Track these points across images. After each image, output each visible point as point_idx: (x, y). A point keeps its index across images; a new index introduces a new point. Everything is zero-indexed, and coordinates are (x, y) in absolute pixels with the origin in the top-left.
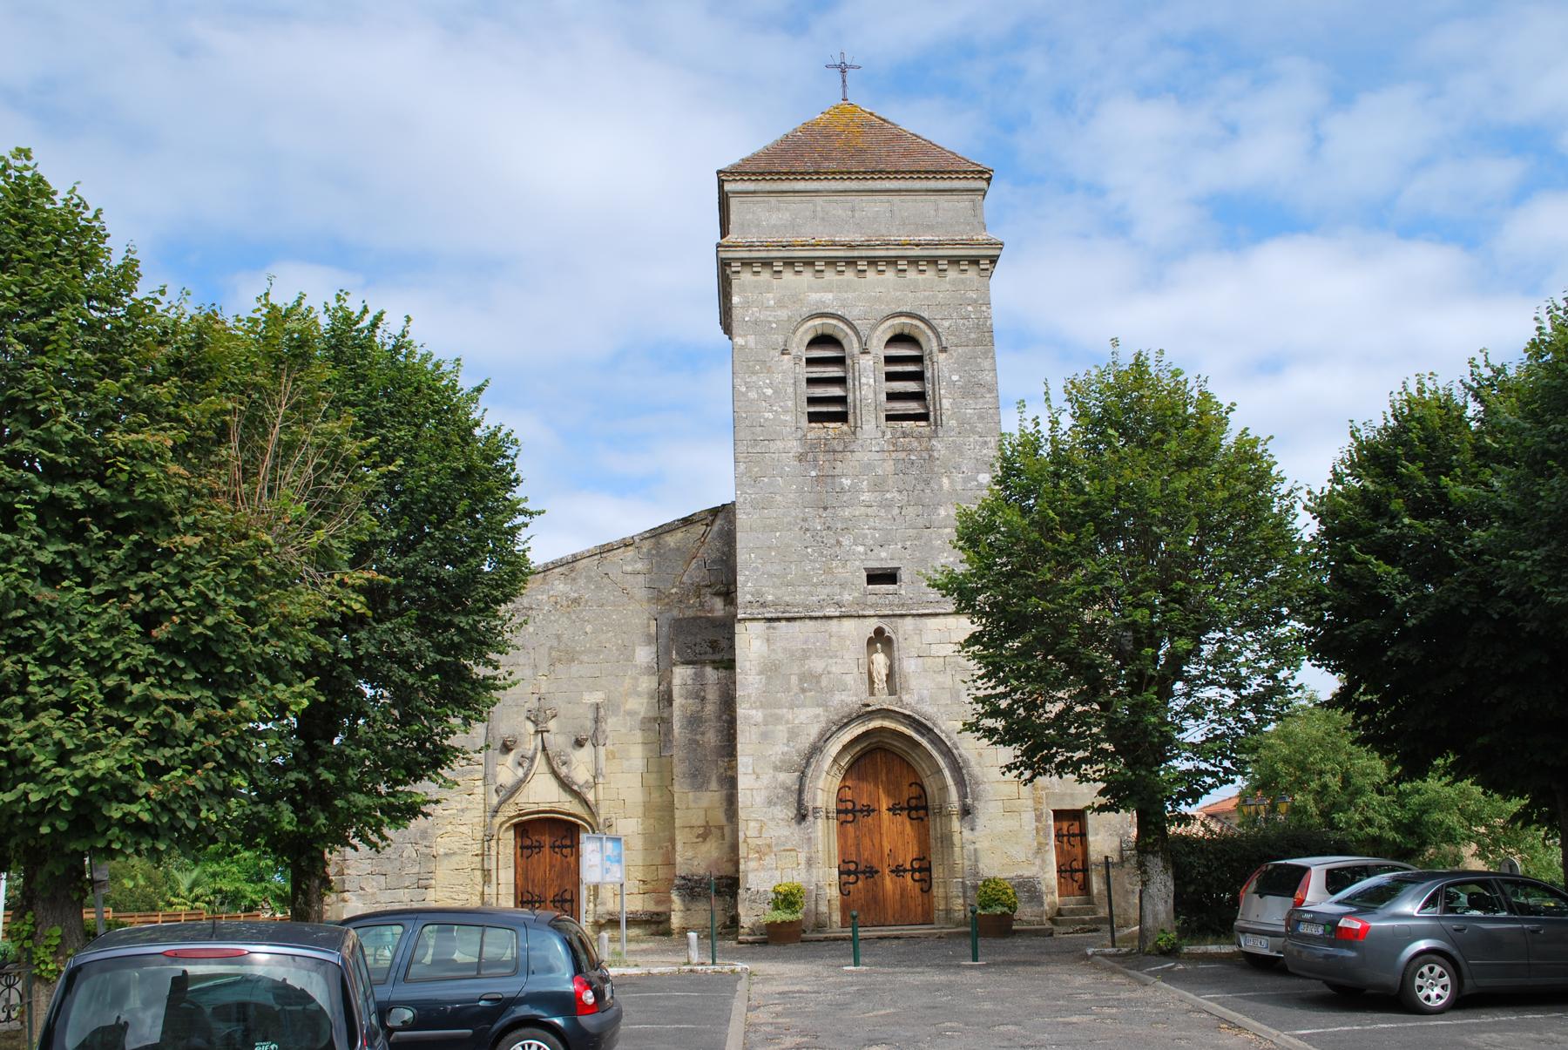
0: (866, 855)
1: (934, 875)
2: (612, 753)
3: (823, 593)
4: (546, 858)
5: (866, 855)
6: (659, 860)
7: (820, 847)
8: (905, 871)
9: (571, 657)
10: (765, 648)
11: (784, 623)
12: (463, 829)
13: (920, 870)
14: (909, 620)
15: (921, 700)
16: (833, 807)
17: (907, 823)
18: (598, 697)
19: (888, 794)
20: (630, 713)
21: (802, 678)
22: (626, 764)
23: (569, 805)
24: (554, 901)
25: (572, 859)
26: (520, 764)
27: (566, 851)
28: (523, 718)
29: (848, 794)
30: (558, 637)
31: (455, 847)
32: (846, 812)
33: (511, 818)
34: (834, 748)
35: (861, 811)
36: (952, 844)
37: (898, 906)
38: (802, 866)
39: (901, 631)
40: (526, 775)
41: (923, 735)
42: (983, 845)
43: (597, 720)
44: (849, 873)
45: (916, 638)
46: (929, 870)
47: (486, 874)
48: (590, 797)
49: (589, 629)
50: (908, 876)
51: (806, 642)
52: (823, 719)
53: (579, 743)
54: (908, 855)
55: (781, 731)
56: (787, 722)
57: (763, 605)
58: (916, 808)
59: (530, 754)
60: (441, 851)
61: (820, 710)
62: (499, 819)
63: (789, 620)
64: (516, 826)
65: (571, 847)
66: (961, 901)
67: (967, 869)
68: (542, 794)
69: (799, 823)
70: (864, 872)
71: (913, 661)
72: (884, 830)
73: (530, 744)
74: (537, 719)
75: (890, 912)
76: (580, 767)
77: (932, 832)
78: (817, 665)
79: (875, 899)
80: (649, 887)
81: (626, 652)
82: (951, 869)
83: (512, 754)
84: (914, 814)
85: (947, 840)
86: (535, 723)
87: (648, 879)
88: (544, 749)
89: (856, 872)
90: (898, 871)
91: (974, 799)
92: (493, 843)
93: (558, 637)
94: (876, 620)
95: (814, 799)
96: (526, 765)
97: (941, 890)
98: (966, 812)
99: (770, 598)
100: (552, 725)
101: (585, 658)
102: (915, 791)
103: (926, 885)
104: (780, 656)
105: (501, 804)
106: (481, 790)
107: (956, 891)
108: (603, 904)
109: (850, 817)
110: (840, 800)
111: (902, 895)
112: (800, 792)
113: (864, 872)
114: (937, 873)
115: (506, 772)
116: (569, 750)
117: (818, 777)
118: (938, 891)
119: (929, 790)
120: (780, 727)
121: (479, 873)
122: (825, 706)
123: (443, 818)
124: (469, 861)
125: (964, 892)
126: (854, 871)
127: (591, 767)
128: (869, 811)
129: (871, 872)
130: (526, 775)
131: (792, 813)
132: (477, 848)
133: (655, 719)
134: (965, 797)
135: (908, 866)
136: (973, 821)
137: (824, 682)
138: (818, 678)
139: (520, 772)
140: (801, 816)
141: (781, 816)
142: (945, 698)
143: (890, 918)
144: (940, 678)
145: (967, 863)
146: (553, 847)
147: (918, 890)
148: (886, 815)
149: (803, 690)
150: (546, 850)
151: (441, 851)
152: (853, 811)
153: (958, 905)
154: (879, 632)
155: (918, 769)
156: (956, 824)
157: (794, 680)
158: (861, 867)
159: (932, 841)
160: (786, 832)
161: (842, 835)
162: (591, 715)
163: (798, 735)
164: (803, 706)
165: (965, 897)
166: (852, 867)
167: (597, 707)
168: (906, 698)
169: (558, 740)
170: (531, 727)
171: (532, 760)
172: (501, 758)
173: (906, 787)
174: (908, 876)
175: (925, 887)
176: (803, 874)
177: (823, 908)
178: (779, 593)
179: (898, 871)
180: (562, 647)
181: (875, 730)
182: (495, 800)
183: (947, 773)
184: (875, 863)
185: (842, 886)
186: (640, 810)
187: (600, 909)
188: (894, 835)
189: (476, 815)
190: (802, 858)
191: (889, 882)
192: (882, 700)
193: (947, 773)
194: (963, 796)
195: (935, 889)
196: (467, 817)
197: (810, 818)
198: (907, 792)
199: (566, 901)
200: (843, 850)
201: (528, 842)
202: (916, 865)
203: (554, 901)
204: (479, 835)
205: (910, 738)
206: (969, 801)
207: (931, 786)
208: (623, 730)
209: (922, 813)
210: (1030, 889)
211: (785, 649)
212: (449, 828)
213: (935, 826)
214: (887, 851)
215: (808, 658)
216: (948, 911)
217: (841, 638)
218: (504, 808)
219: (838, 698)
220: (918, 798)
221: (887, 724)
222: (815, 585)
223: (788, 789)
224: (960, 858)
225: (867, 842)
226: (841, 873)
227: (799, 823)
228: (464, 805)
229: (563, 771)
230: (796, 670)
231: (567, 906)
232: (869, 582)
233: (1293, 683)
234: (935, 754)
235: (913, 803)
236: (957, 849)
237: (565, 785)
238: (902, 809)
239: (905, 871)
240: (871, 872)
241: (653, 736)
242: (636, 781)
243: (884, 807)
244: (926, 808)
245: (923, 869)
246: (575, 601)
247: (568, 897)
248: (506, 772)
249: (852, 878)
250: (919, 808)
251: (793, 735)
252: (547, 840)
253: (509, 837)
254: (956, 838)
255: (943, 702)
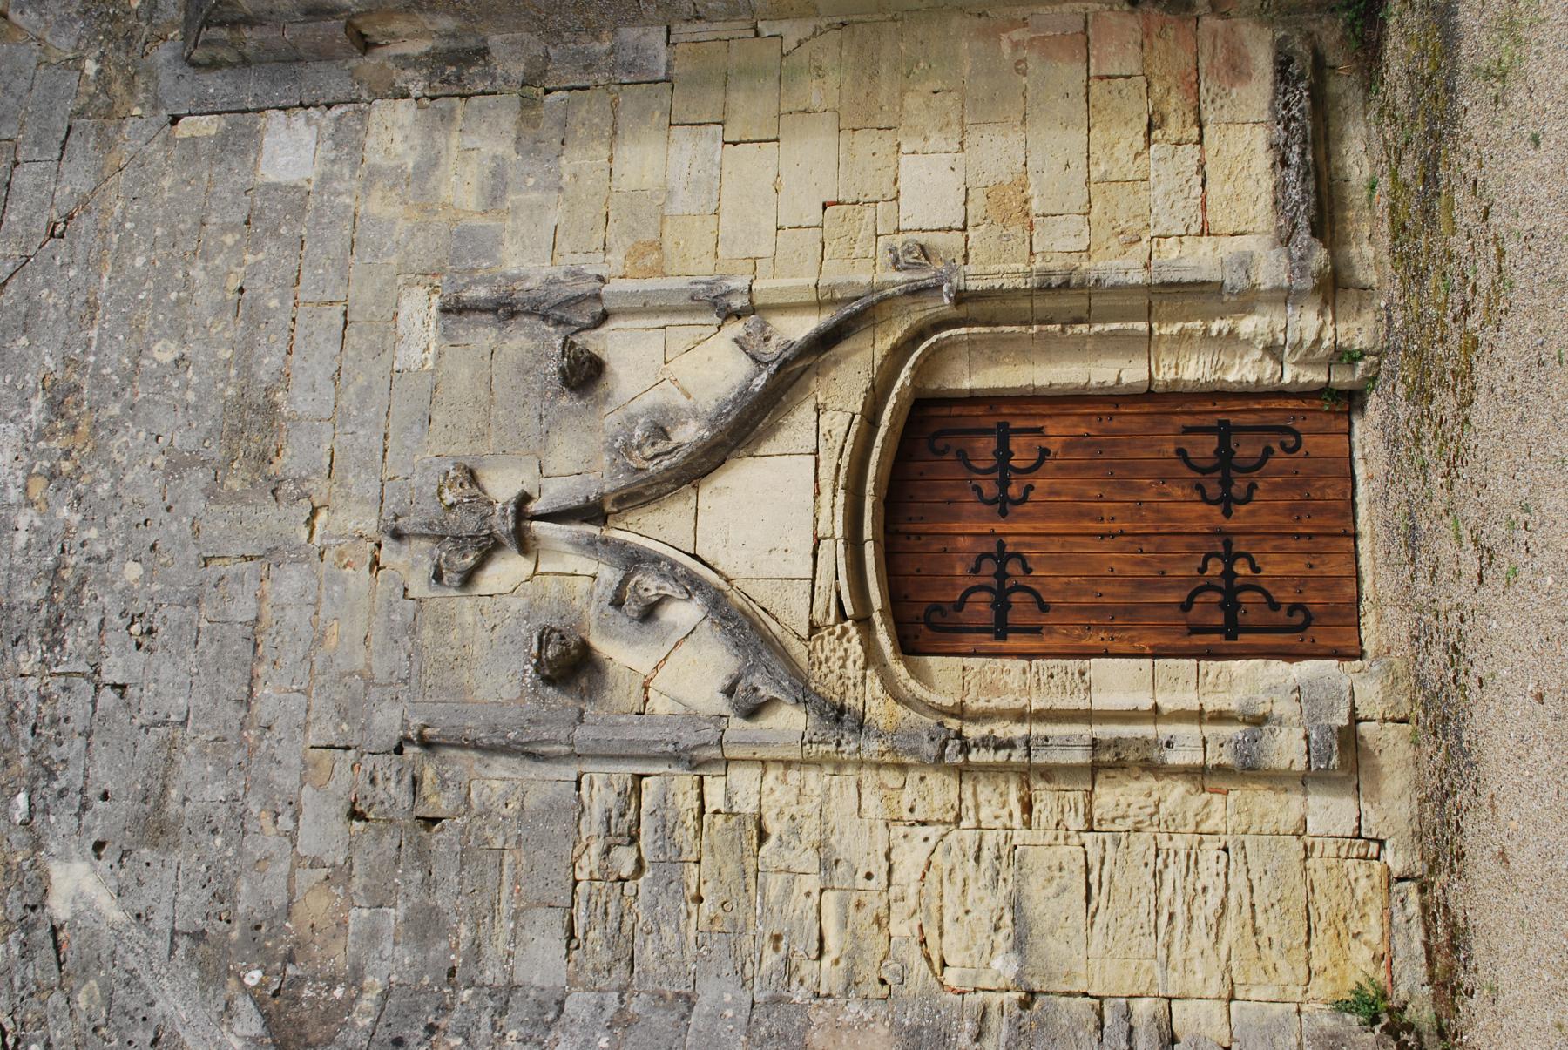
2: (638, 252)
4: (1055, 531)
6: (1069, 74)
9: (255, 418)
12: (909, 860)
18: (418, 310)
20: (496, 190)
22: (683, 202)
23: (844, 388)
24: (1227, 503)
25: (1057, 430)
26: (649, 613)
27: (1022, 451)
28: (464, 607)
30: (178, 465)
31: (987, 903)
33: (872, 656)
40: (694, 585)
43: (505, 310)
47: (1108, 762)
48: (799, 328)
49: (164, 352)
53: (584, 375)
59: (610, 575)
60: (1004, 966)
62: (879, 708)
63: (332, 747)
64: (908, 647)
65: (1004, 434)
68: (776, 522)
73: (571, 572)
74: (478, 539)
76: (680, 372)
80: (1174, 105)
81: (274, 215)
83: (604, 647)
86: (489, 549)
87: (1139, 110)
88: (591, 512)
92: (973, 731)
93: (178, 465)
96: (651, 585)
100: (502, 486)
101: (269, 362)
105: (805, 694)
106: (744, 780)
108: (1245, 263)
115: (677, 670)
116: (610, 420)
121: (1109, 797)
123: (853, 956)
124: (1051, 848)
127: (683, 331)
130: (694, 585)
132: (995, 803)
133: (528, 103)
139: (684, 613)
146: (1003, 506)
150: (1014, 528)
151: (1004, 966)
162: (484, 335)
167: (455, 309)
169: (573, 463)
170: (507, 570)
171: (634, 560)
172: (622, 693)
180: (216, 451)
182: (789, 720)
186: (866, 143)
187: (1270, 270)
189: (853, 809)
196: (858, 844)
199: (1225, 453)
201: (981, 607)
203: (1227, 503)
204: (938, 791)
208: (556, 215)
212: (901, 927)
218: (828, 684)
228: (807, 860)
229: (689, 434)
231: (1246, 449)
237: (745, 426)
241: (590, 110)
242: (753, 164)
246: (56, 407)
247: (1206, 447)
248: (677, 670)
252: (971, 528)
253: (949, 677)
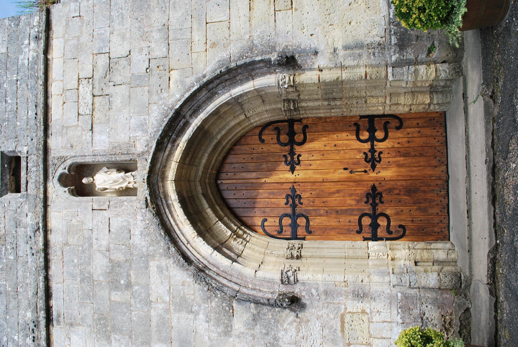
0: (351, 202)
1: (380, 110)
3: (24, 249)
5: (351, 202)
7: (339, 278)
8: (372, 150)
10: (81, 330)
11: (53, 302)
13: (372, 130)
14: (52, 142)
15: (142, 126)
16: (281, 246)
17: (308, 146)
19: (271, 170)
21: (114, 285)
29: (272, 223)
32: (294, 226)
34: (200, 249)
35: (294, 206)
36: (338, 83)
37: (422, 161)
38: (366, 306)
39: (64, 153)
41: (187, 124)
42: (339, 38)
44: (375, 226)
45: (71, 133)
46: (371, 118)
50: (379, 146)
51: (73, 277)
52: (165, 262)
54: (351, 146)
55: (180, 320)
56: (167, 311)
57: (36, 325)
58: (292, 134)
61: (153, 265)
66: (422, 69)
67: (373, 61)
69: (303, 307)
70: (374, 206)
71: (97, 137)
72: (319, 177)
75: (429, 171)
77: (322, 114)
78: (99, 265)
79: (410, 191)
82: (373, 83)
84: (299, 138)
85: (332, 90)
89: (374, 217)
90: (373, 160)
91: (273, 49)
94: (50, 185)
95: (271, 281)
97: (402, 100)
98: (289, 62)
99: (29, 315)
102: (269, 136)
103: (392, 122)
104: (88, 311)
107: (407, 74)
109: (301, 221)
110: (278, 235)
111: (406, 155)
112: (257, 303)
113: (374, 206)
114: (377, 106)
117: (240, 275)
118: (403, 105)
119: (266, 118)
120: (174, 322)
122: (147, 257)
125: (409, 63)
126: (375, 216)
128: (294, 197)
129: (374, 195)
131: (288, 316)
134: (267, 63)
135: (367, 146)
136: (304, 52)
137: (119, 257)
138: (114, 265)
140: (294, 302)
141: (293, 331)
142: (141, 94)
143: (438, 172)
144: (117, 101)
145: (364, 60)
147: (399, 134)
148: (300, 174)
149: (129, 285)
152: (294, 216)
153: (427, 73)
154: (63, 180)
155: (239, 131)
156: (308, 77)
157: (117, 296)
158: (367, 209)
159: (335, 113)
160: (315, 326)
161: (325, 233)
163: (184, 299)
164: (147, 287)
165: (416, 62)
166: (367, 221)
168: (140, 148)
173: (265, 148)
174: (379, 146)
175: (394, 123)
176: (379, 305)
177: (432, 279)
178: (24, 303)
179: (373, 160)
181: (179, 193)
183: (237, 91)
184: (362, 190)
185: (395, 235)
188: (326, 163)
190: (353, 305)
191: (386, 173)
192: (138, 179)
193: (237, 91)
194: (268, 67)
195: (401, 110)
197: (297, 290)
198: (272, 146)
200: (344, 233)
202: (365, 135)
205: (190, 142)
206: (274, 57)
207: (261, 114)
209: (297, 127)
210: (299, 312)
211: (82, 305)
213: (313, 107)
214: (346, 174)
215: (91, 276)
216: (433, 89)
217: (69, 231)
219: (138, 240)
220: (278, 131)
221: (171, 173)
222: (17, 257)
223: (255, 319)
224: (358, 69)
225: (334, 201)
226: (375, 238)
227: (303, 307)
230: (104, 293)
232: (20, 192)
233: (434, 341)
234: (211, 108)
235: (284, 138)
236: (345, 75)
238: (292, 153)
239: (372, 150)
240: (374, 195)
243: (289, 176)
244: (291, 122)
245: (370, 125)
249: (382, 222)
250: (291, 130)
251: (183, 305)
254: (328, 76)
255: (146, 98)
